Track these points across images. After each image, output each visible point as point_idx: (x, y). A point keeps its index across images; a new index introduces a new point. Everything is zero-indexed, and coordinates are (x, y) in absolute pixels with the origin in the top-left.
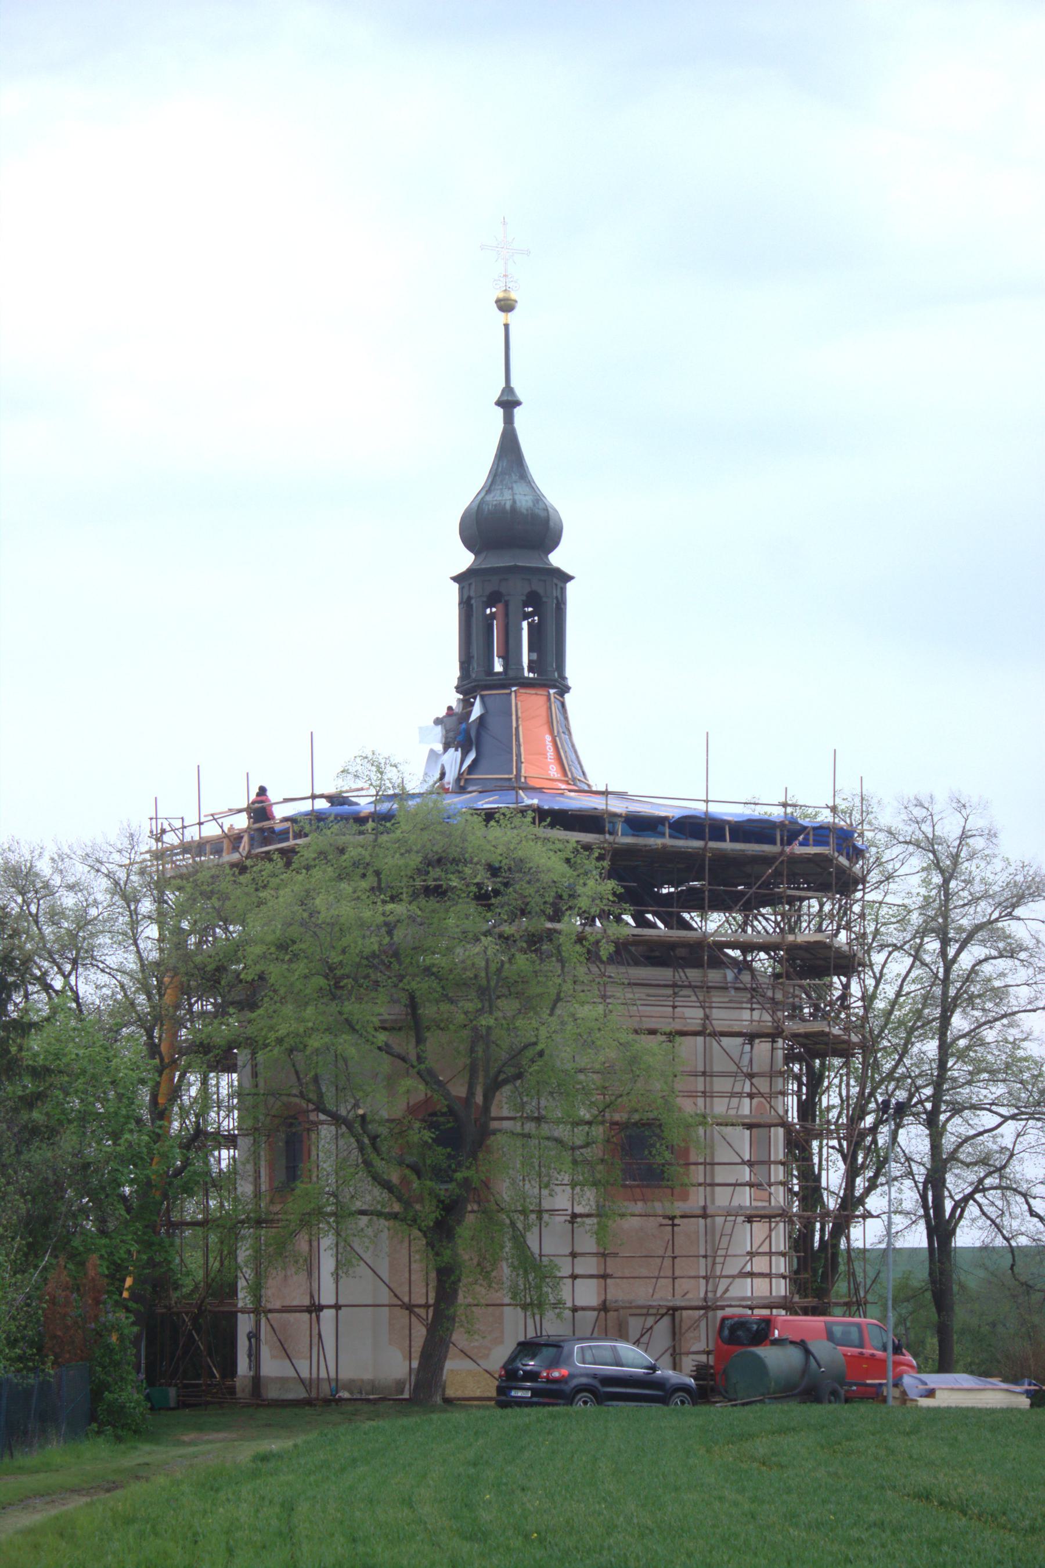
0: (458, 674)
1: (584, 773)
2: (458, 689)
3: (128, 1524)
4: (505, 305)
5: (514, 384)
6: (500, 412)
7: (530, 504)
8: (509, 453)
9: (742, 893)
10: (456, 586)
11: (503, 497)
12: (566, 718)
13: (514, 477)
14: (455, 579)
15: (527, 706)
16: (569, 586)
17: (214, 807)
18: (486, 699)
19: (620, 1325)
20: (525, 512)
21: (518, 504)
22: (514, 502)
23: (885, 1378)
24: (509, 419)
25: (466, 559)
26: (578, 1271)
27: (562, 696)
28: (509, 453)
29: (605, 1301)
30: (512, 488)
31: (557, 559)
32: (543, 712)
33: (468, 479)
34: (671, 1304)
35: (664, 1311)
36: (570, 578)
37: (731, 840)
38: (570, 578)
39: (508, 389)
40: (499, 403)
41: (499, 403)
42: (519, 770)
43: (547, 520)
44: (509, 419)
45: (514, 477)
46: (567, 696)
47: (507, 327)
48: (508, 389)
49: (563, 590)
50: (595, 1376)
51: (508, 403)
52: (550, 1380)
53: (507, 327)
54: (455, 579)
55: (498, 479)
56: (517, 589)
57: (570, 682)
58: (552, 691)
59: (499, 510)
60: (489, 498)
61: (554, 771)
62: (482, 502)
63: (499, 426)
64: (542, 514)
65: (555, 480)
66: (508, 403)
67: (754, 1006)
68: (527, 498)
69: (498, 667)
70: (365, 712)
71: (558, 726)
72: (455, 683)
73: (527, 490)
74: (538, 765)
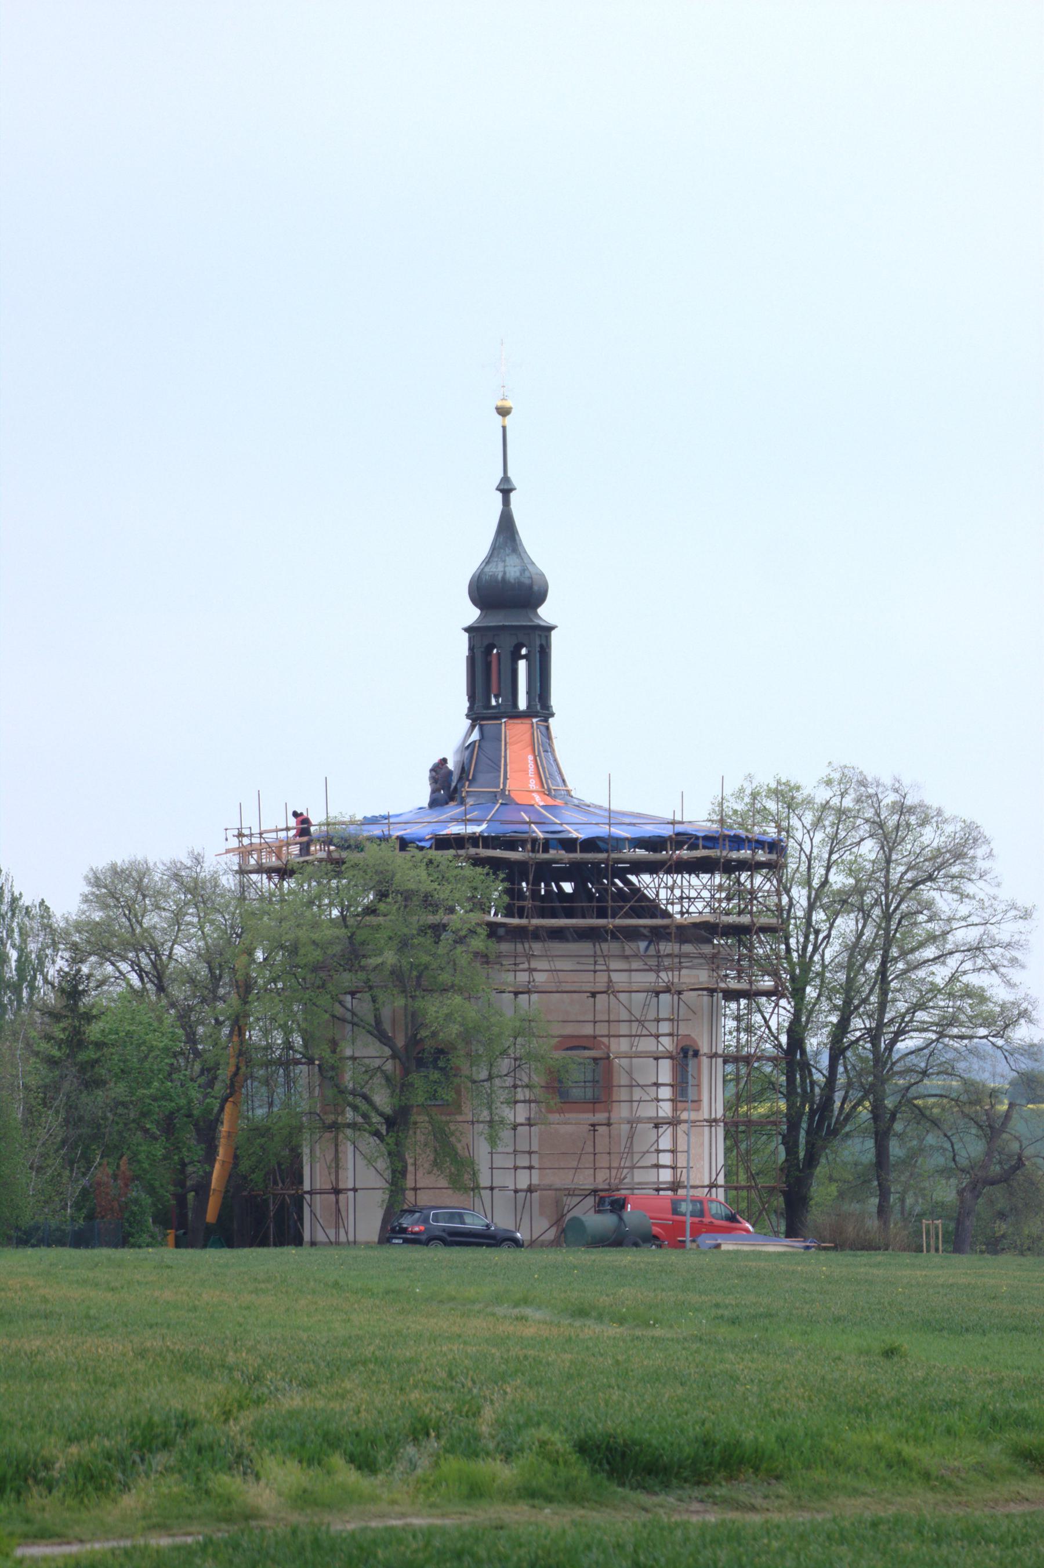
0: (467, 704)
1: (564, 781)
2: (468, 716)
3: (649, 1474)
4: (503, 412)
5: (510, 474)
6: (499, 495)
7: (518, 574)
8: (507, 528)
9: (603, 883)
10: (465, 636)
11: (497, 570)
12: (549, 737)
13: (508, 551)
14: (466, 630)
15: (515, 735)
16: (553, 633)
17: (274, 821)
18: (484, 727)
19: (557, 1202)
20: (512, 581)
21: (508, 575)
22: (505, 573)
23: (684, 1236)
24: (506, 502)
25: (472, 614)
26: (519, 1164)
27: (546, 720)
28: (507, 528)
29: (530, 1185)
30: (504, 561)
31: (546, 613)
32: (527, 737)
33: (473, 550)
34: (592, 1187)
35: (587, 1192)
36: (550, 628)
37: (581, 852)
38: (550, 628)
39: (506, 479)
40: (497, 489)
41: (497, 489)
42: (505, 784)
43: (530, 587)
44: (506, 502)
45: (508, 551)
46: (551, 720)
47: (504, 428)
48: (506, 479)
49: (548, 639)
50: (444, 1231)
51: (506, 490)
52: (413, 1233)
53: (504, 428)
54: (466, 630)
55: (496, 552)
56: (508, 642)
57: (554, 709)
58: (535, 720)
59: (493, 578)
60: (487, 569)
61: (533, 784)
62: (479, 577)
63: (499, 507)
64: (527, 581)
65: (542, 549)
66: (506, 490)
67: (598, 967)
68: (516, 569)
69: (494, 703)
70: (377, 744)
71: (543, 746)
72: (466, 711)
73: (517, 561)
74: (521, 779)
